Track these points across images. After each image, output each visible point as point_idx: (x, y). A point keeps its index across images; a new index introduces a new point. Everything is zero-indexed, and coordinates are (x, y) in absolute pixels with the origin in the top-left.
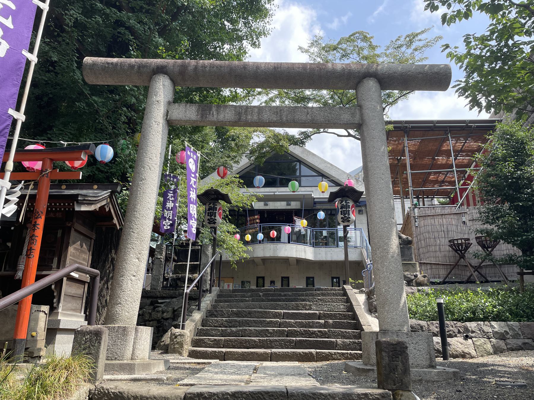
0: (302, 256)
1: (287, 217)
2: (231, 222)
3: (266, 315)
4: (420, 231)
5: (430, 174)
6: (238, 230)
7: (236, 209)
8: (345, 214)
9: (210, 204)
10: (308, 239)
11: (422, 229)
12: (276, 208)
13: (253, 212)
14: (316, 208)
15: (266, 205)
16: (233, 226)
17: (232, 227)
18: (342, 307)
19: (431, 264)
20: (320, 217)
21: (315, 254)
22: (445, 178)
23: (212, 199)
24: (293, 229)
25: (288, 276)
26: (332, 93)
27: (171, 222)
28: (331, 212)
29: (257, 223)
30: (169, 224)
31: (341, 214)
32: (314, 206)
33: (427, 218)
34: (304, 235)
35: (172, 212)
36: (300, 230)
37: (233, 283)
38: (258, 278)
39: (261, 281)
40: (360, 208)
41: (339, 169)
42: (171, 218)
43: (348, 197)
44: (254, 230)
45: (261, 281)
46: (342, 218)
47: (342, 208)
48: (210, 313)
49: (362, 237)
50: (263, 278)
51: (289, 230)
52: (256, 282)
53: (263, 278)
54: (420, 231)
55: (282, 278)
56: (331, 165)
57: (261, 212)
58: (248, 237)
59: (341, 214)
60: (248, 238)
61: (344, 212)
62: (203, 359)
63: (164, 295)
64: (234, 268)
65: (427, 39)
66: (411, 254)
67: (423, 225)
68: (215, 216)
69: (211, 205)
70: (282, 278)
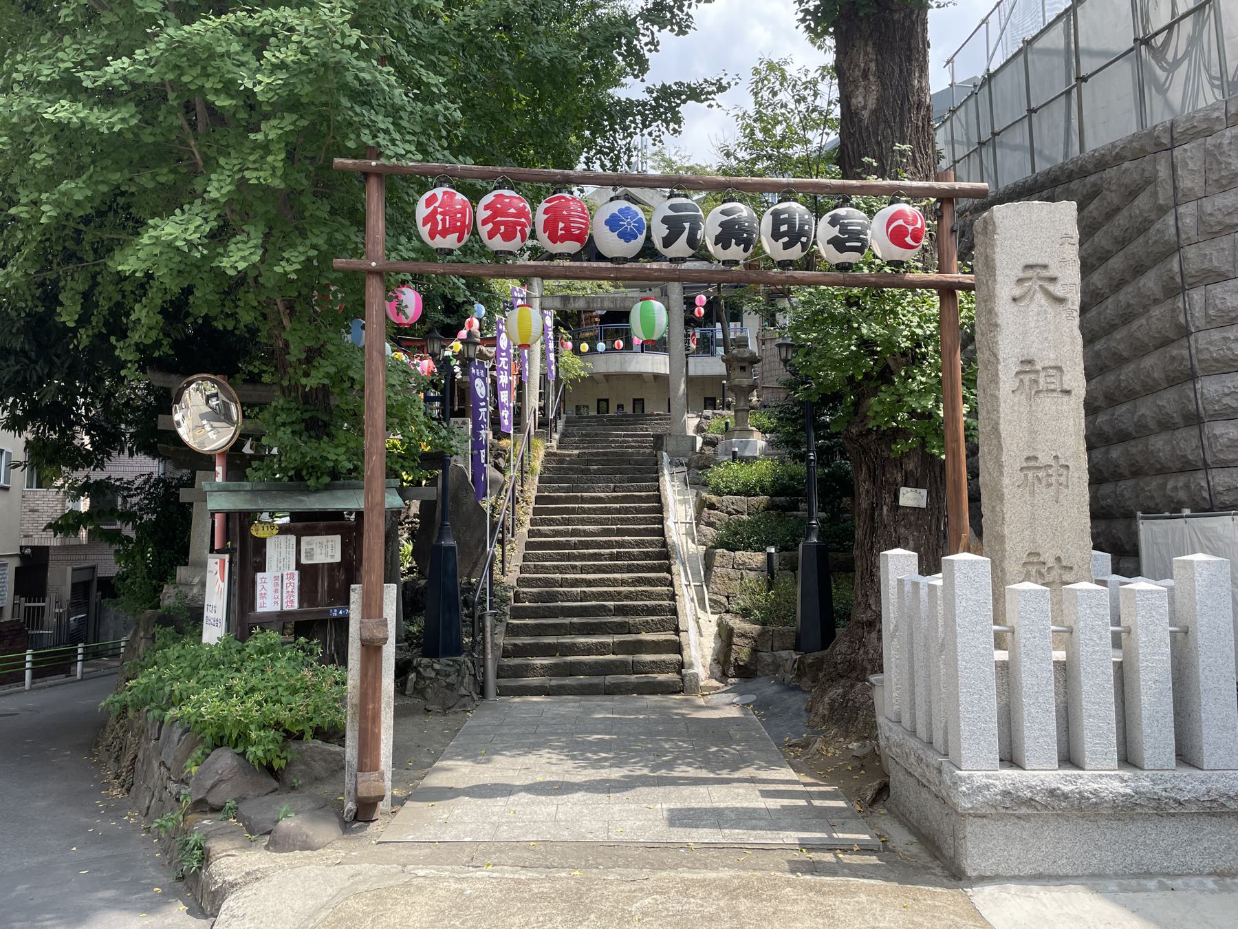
3: (611, 436)
5: (494, 645)
26: (498, 317)
39: (603, 404)
45: (603, 404)
48: (563, 435)
50: (607, 401)
53: (607, 401)
58: (585, 347)
62: (396, 748)
65: (1045, 267)
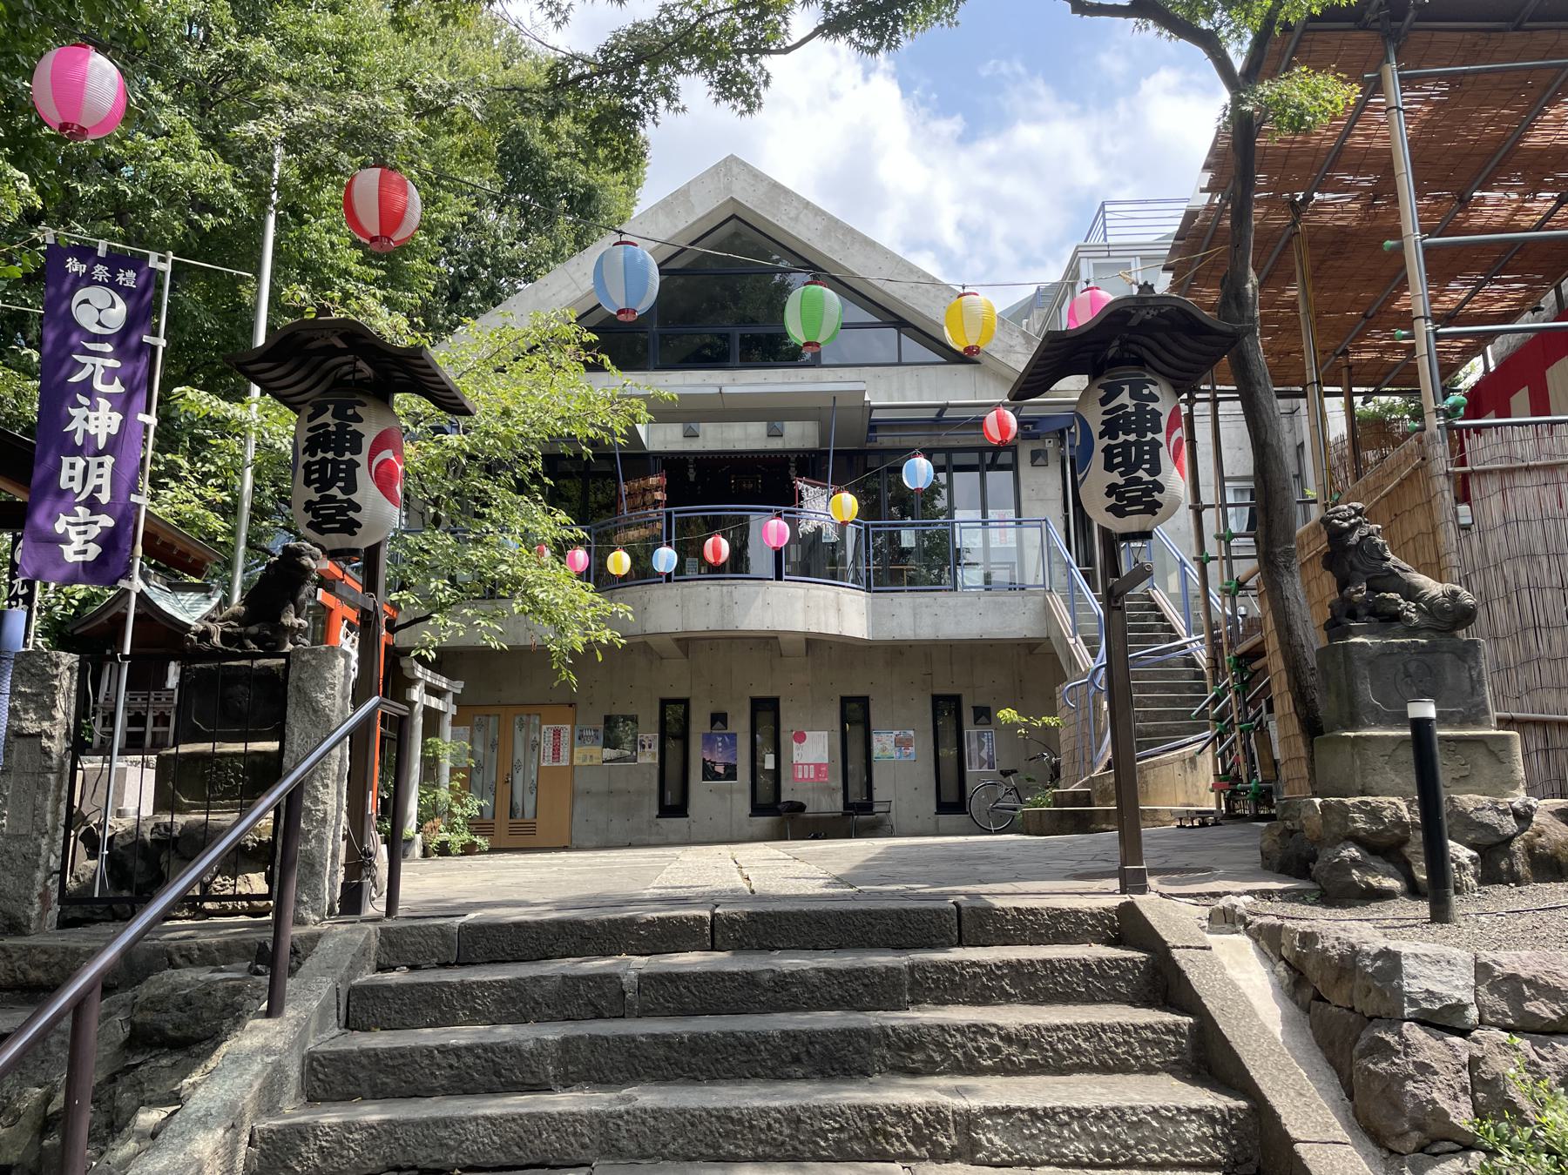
1: (770, 479)
2: (555, 499)
4: (1484, 551)
6: (583, 534)
7: (563, 449)
8: (1130, 467)
9: (319, 410)
10: (850, 558)
11: (1492, 540)
13: (638, 461)
15: (690, 435)
16: (562, 517)
17: (552, 523)
18: (1192, 1129)
19: (1544, 723)
21: (874, 615)
22: (1467, 300)
23: (339, 384)
24: (794, 524)
25: (775, 694)
27: (107, 521)
28: (994, 459)
29: (656, 503)
30: (95, 531)
31: (1109, 467)
32: (869, 440)
33: (1520, 480)
35: (108, 460)
36: (819, 530)
40: (1037, 445)
42: (104, 497)
43: (1140, 362)
44: (643, 532)
46: (1112, 490)
47: (1110, 429)
49: (1047, 547)
51: (780, 536)
52: (656, 717)
54: (1484, 551)
57: (673, 464)
58: (620, 562)
59: (1109, 467)
60: (618, 563)
61: (322, 471)
63: (34, 974)
64: (567, 683)
66: (1476, 684)
67: (1498, 520)
68: (351, 487)
69: (327, 418)
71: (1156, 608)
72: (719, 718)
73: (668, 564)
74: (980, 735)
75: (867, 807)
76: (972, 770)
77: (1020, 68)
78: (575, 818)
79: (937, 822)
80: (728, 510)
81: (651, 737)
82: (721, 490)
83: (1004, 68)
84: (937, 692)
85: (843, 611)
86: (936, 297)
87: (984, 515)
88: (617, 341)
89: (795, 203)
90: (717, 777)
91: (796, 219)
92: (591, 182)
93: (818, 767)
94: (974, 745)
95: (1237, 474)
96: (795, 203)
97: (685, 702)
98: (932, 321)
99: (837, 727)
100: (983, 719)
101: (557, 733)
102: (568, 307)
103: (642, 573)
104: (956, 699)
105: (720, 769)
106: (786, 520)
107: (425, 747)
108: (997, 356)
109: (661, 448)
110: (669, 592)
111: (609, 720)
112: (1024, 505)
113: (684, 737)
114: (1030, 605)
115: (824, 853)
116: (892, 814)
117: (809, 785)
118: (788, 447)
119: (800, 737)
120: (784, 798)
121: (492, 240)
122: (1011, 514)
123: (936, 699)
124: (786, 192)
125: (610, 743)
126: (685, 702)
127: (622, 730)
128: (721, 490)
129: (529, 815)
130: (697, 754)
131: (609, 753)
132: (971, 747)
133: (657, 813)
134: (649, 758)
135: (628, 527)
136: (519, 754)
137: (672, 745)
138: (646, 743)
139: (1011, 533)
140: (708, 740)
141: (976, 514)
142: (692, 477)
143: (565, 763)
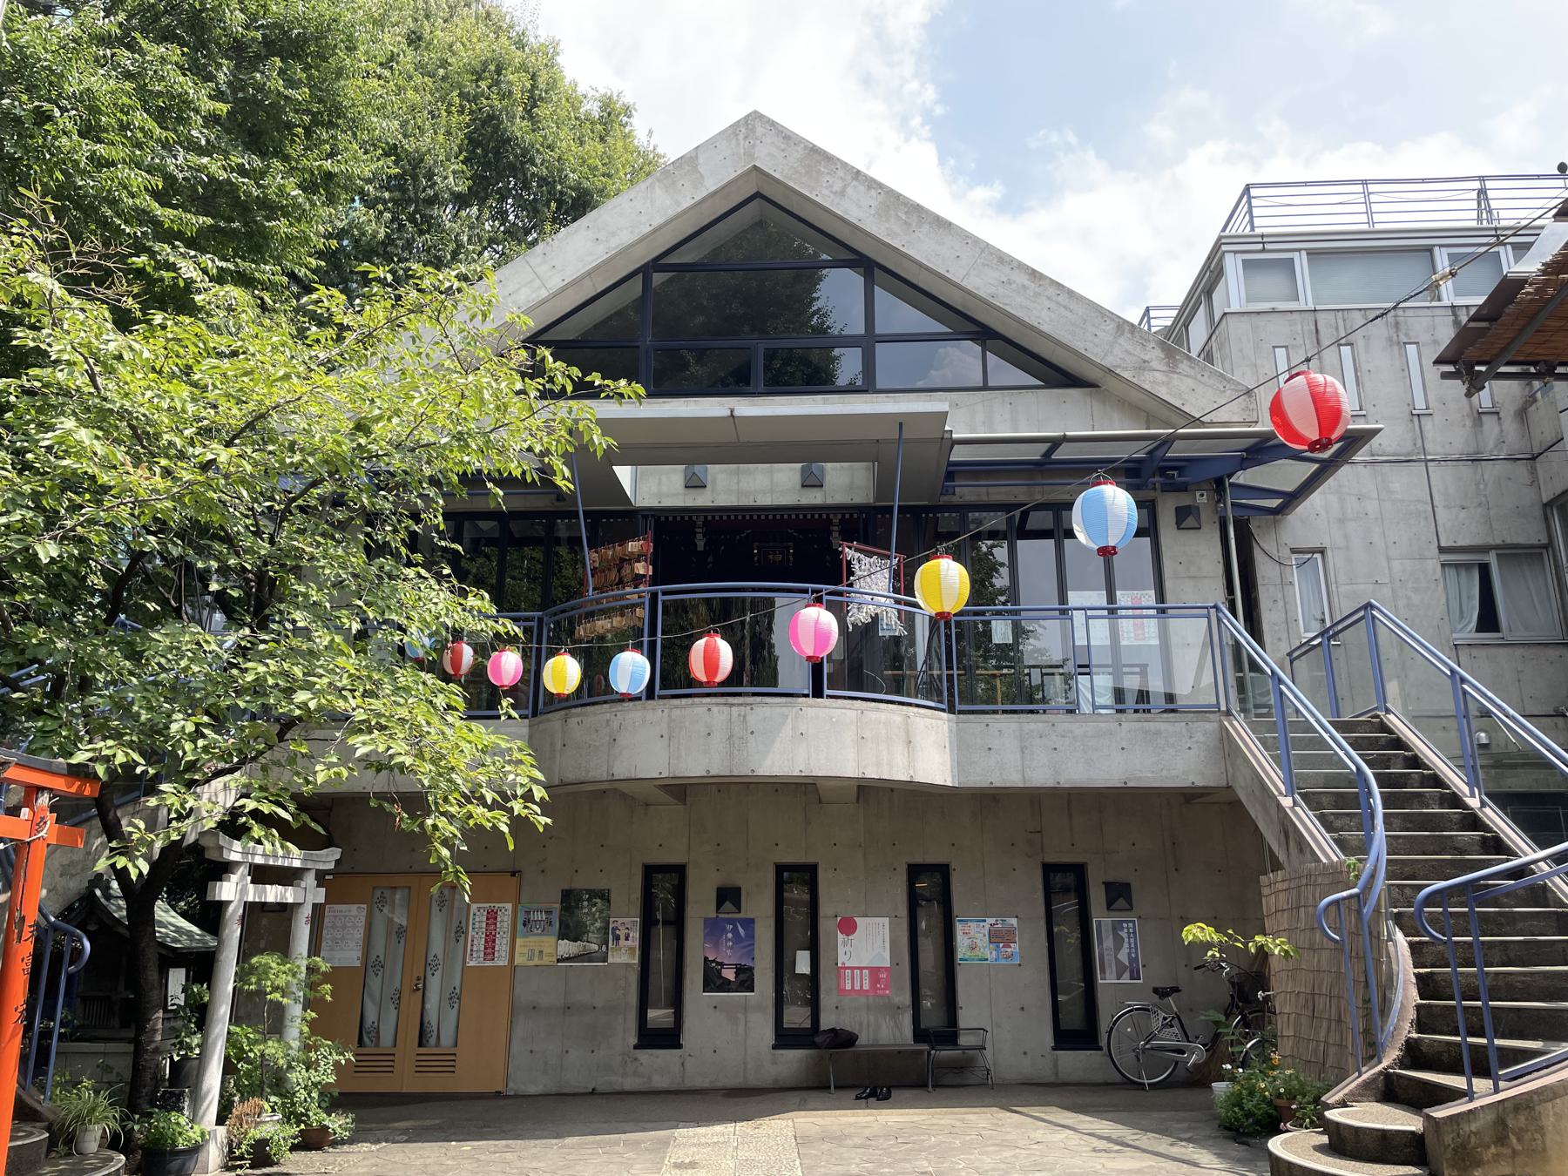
0: (896, 769)
1: (805, 549)
2: (465, 576)
12: (747, 502)
13: (619, 520)
14: (955, 500)
20: (499, 677)
21: (961, 749)
25: (811, 860)
29: (637, 580)
32: (945, 491)
34: (897, 640)
37: (517, 902)
38: (650, 871)
40: (1184, 500)
41: (1071, 293)
44: (617, 621)
52: (637, 895)
55: (780, 869)
56: (1034, 274)
60: (560, 675)
70: (780, 869)
71: (1399, 743)
72: (728, 896)
73: (634, 679)
74: (1116, 927)
75: (948, 1034)
76: (1106, 980)
77: (1072, 139)
78: (515, 1047)
79: (1056, 1062)
80: (746, 589)
81: (629, 926)
82: (730, 564)
83: (1054, 138)
84: (1052, 858)
85: (915, 745)
86: (1037, 294)
87: (1111, 598)
88: (588, 344)
89: (840, 173)
90: (725, 986)
91: (842, 193)
92: (586, 184)
93: (874, 971)
94: (1109, 943)
95: (1460, 543)
96: (840, 173)
97: (680, 870)
98: (1032, 328)
99: (903, 911)
100: (1121, 902)
101: (492, 916)
102: (525, 313)
103: (595, 686)
104: (1079, 870)
105: (729, 974)
106: (830, 607)
107: (241, 977)
108: (1126, 375)
109: (655, 504)
110: (650, 716)
111: (570, 900)
112: (1168, 585)
113: (678, 923)
114: (1199, 737)
115: (894, 1135)
116: (988, 1053)
117: (863, 1000)
118: (830, 501)
119: (848, 927)
120: (824, 1026)
121: (452, 246)
122: (1149, 597)
123: (1049, 870)
124: (828, 158)
125: (570, 931)
126: (680, 870)
127: (589, 913)
128: (730, 564)
129: (447, 1038)
130: (697, 949)
131: (567, 947)
132: (1103, 946)
133: (634, 1040)
134: (625, 954)
135: (590, 615)
136: (437, 947)
137: (661, 934)
138: (622, 933)
139: (1152, 626)
140: (713, 929)
141: (1098, 598)
142: (701, 545)
143: (502, 962)
